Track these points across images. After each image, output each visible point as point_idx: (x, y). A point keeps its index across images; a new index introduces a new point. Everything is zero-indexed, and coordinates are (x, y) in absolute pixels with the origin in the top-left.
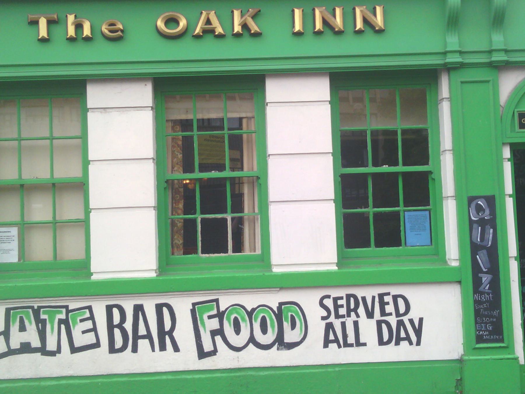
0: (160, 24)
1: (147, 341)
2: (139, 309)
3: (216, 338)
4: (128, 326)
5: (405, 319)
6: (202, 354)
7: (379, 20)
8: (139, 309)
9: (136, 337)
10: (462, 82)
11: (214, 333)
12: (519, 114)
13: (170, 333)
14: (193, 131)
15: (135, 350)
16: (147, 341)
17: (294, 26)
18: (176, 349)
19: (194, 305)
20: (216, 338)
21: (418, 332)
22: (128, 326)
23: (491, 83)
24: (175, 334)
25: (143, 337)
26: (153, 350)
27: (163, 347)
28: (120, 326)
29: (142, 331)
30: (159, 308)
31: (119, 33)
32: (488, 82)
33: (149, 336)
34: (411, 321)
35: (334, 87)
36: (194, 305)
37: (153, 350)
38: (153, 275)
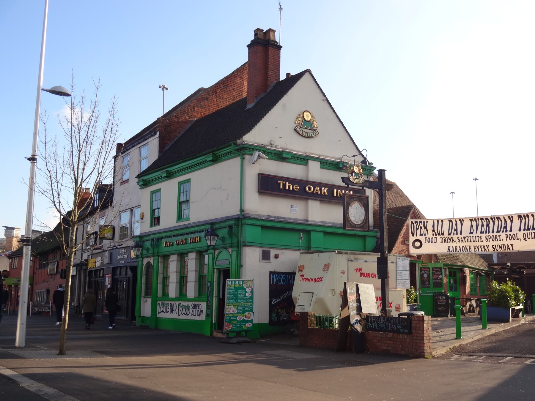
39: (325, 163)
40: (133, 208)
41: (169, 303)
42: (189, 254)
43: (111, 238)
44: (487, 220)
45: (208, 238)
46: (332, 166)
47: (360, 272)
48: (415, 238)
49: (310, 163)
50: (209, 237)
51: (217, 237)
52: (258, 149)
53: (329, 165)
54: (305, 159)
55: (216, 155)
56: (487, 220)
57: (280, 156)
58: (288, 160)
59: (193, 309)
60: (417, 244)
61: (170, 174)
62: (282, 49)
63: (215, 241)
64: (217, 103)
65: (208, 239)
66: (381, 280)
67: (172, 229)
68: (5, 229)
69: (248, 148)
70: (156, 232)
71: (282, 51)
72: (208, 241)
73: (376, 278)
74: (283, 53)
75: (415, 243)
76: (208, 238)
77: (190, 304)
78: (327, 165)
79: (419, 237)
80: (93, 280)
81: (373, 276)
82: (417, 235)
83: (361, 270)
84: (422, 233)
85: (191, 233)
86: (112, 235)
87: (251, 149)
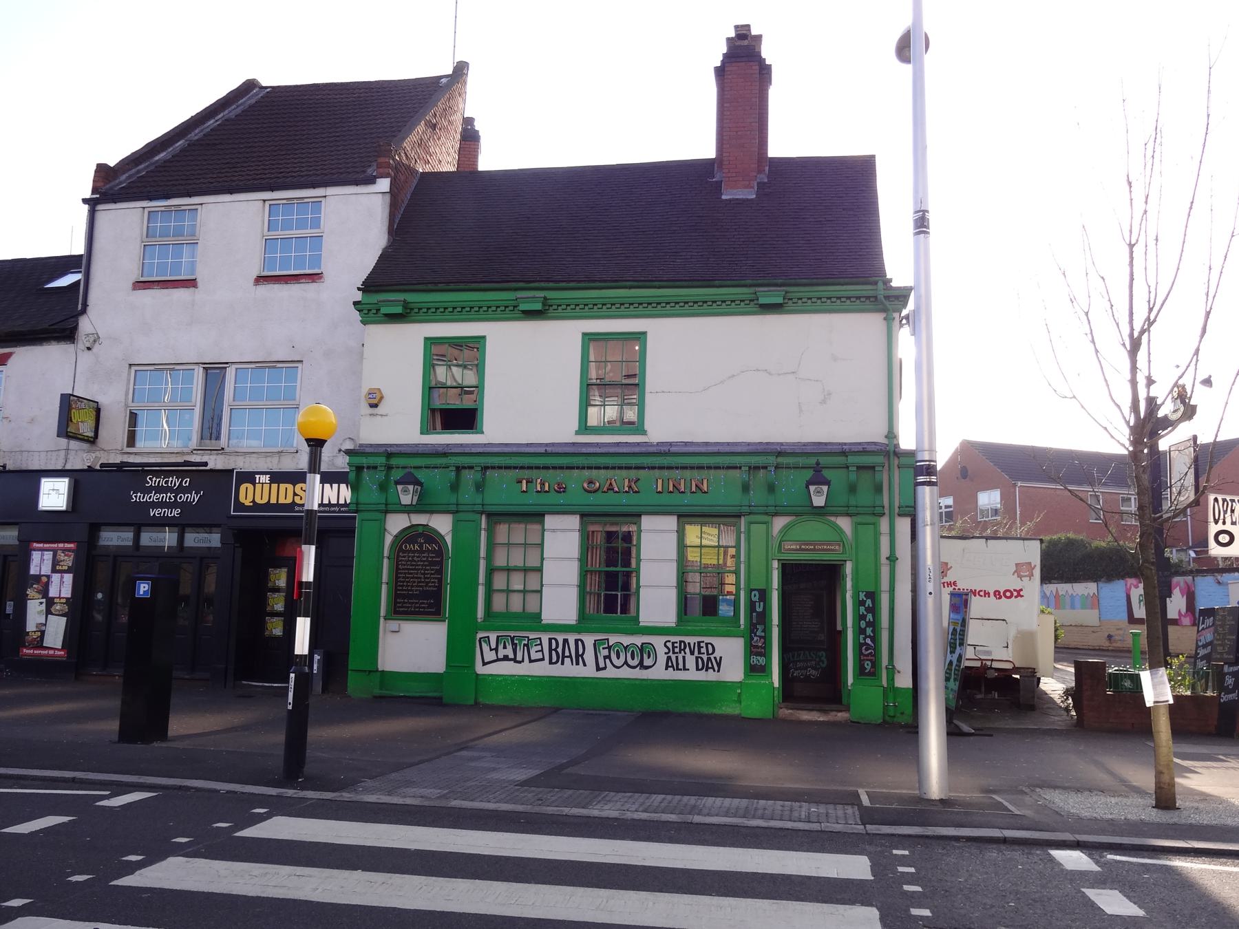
40: (227, 363)
41: (545, 639)
42: (643, 517)
43: (91, 437)
47: (953, 587)
48: (1220, 527)
49: (1151, 394)
51: (413, 486)
55: (548, 301)
59: (674, 653)
60: (1224, 538)
61: (409, 311)
63: (410, 493)
64: (719, 224)
66: (296, 653)
67: (474, 450)
68: (1159, 402)
70: (420, 450)
73: (989, 597)
75: (1219, 535)
77: (658, 642)
79: (1228, 527)
81: (982, 593)
82: (1224, 523)
83: (955, 583)
84: (1234, 521)
85: (590, 468)
86: (93, 430)
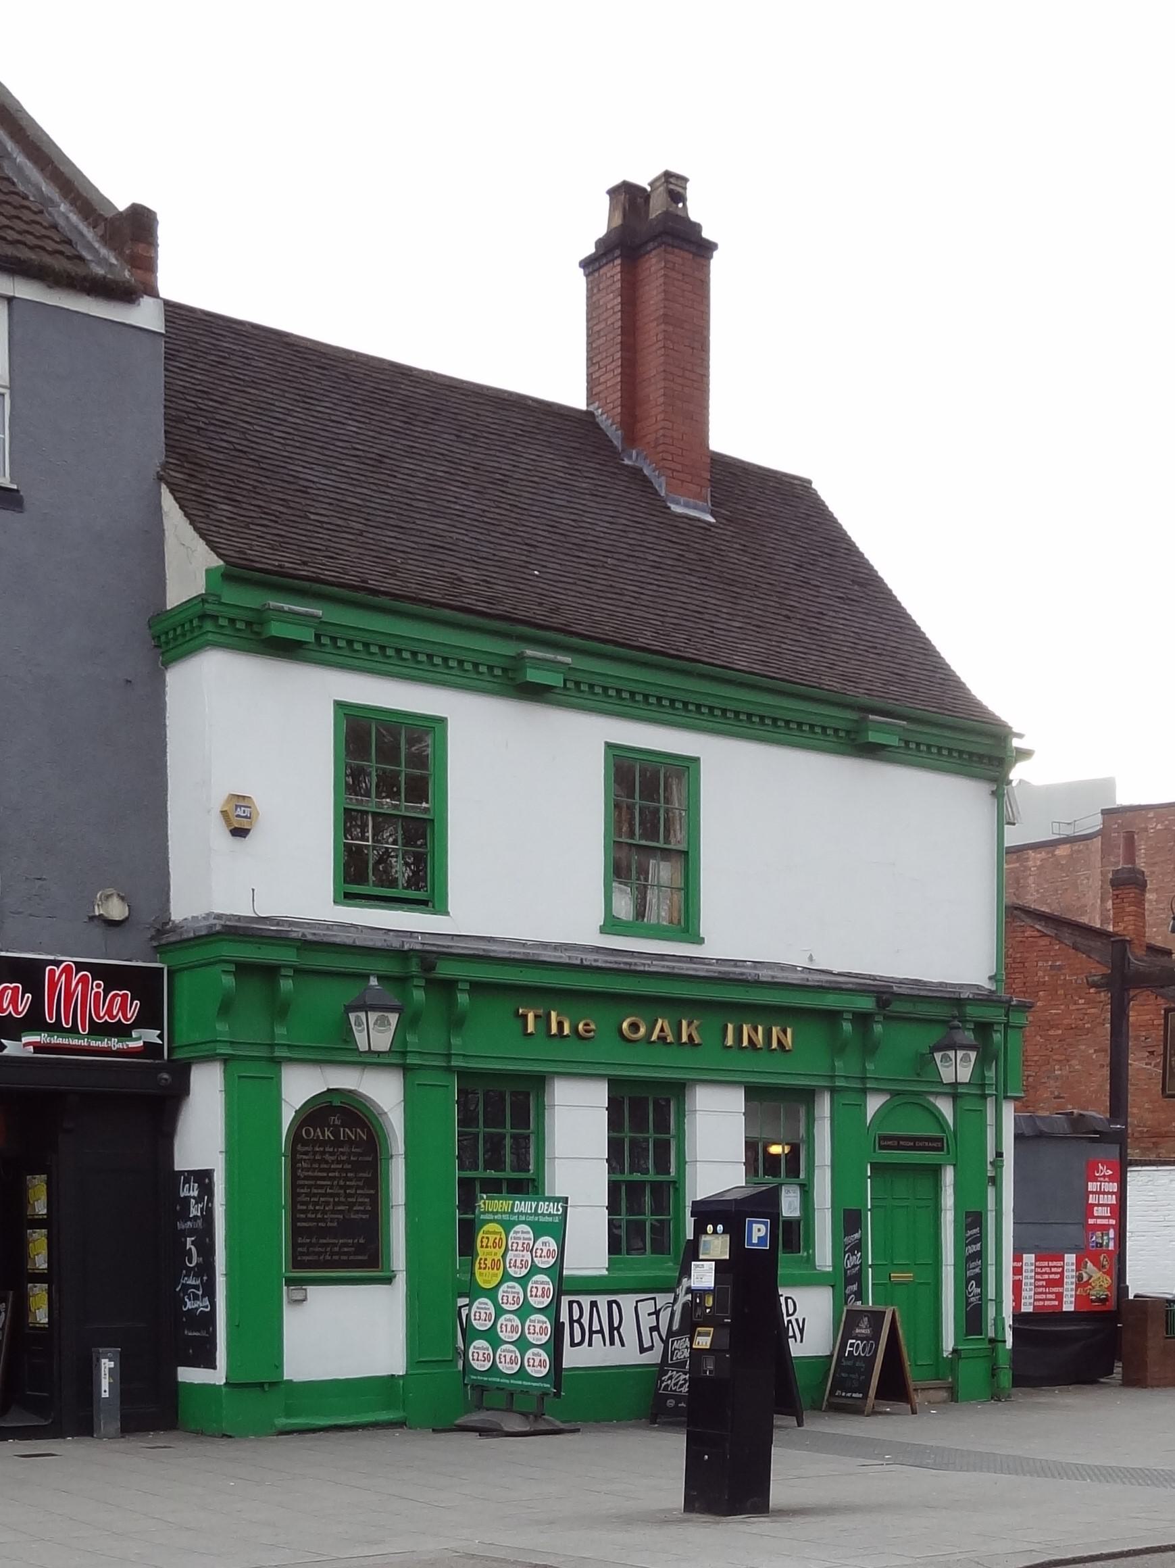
0: (625, 1025)
1: (793, 1339)
2: (594, 1304)
3: (653, 1333)
4: (585, 1321)
5: (793, 1318)
6: (643, 1350)
7: (789, 1041)
8: (594, 1304)
9: (592, 1332)
10: (240, 1077)
11: (652, 1329)
12: (879, 1137)
13: (618, 1329)
14: (478, 1127)
15: (590, 1345)
16: (793, 1339)
17: (527, 1029)
18: (623, 1345)
19: (637, 1302)
20: (653, 1333)
21: (801, 1331)
22: (585, 1321)
23: (275, 1079)
24: (621, 1330)
25: (597, 1332)
26: (605, 1344)
27: (612, 1343)
28: (579, 1321)
29: (596, 1327)
30: (610, 1303)
31: (592, 1034)
32: (272, 1078)
33: (601, 1331)
34: (797, 1320)
35: (748, 1099)
36: (637, 1302)
37: (605, 1344)
38: (605, 1273)
39: (704, 710)
44: (595, 1309)
45: (358, 1017)
46: (671, 711)
50: (362, 1015)
52: (338, 635)
53: (960, 757)
54: (714, 708)
56: (595, 1309)
57: (258, 634)
58: (550, 696)
62: (715, 254)
65: (359, 1023)
69: (756, 715)
71: (717, 264)
72: (360, 1031)
74: (719, 268)
76: (358, 1017)
78: (817, 737)
80: (651, 1135)
87: (792, 725)
